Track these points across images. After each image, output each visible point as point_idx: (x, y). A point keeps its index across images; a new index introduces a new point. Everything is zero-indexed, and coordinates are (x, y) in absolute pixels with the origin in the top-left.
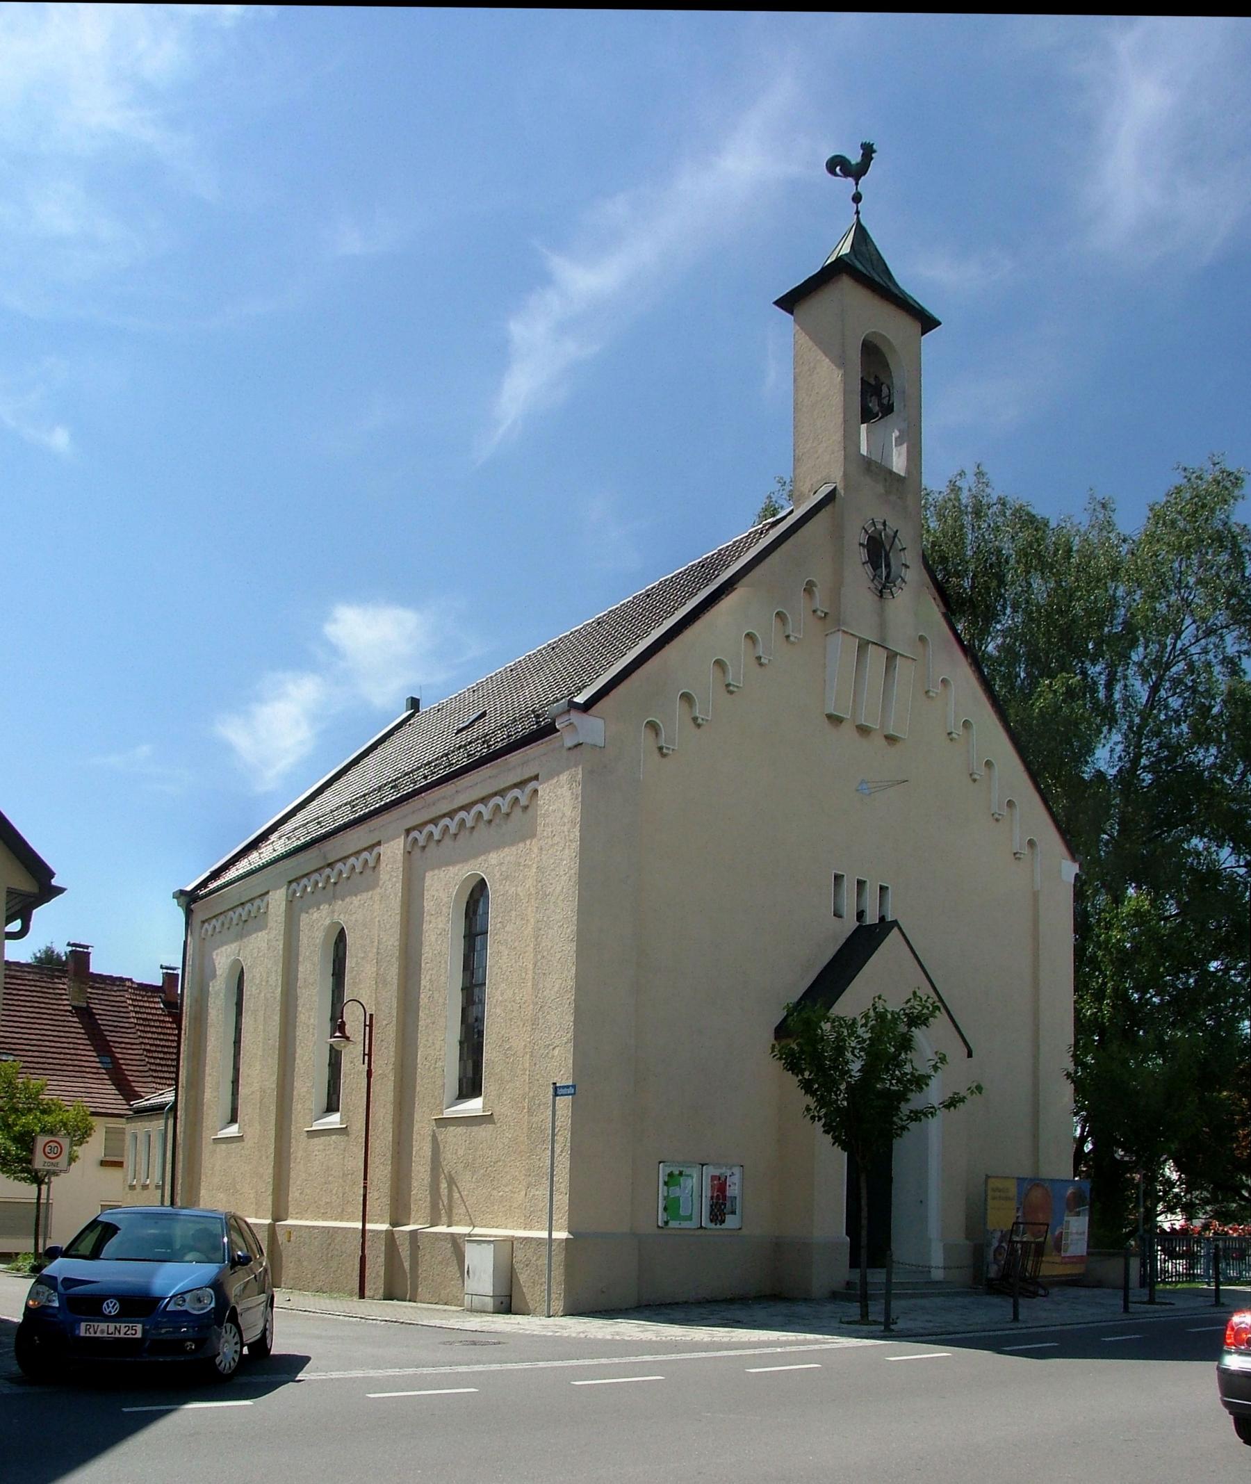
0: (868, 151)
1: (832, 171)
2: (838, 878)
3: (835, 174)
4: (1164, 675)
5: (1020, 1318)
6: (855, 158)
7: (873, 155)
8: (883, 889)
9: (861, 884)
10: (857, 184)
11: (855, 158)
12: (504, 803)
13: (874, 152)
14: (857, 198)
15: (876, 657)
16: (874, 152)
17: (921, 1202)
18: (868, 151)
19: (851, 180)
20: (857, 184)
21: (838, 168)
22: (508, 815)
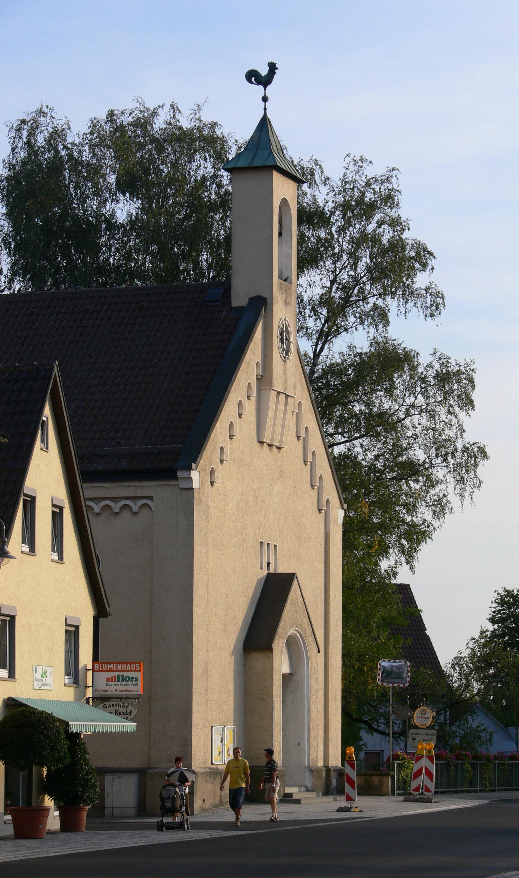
0: (273, 67)
1: (249, 79)
2: (262, 543)
3: (251, 83)
4: (352, 402)
5: (195, 813)
6: (264, 71)
7: (276, 71)
8: (275, 546)
9: (268, 544)
10: (265, 90)
11: (264, 71)
12: (116, 507)
13: (277, 68)
14: (265, 99)
15: (282, 397)
16: (277, 68)
17: (299, 744)
18: (273, 67)
19: (261, 87)
20: (265, 90)
21: (253, 78)
22: (117, 514)
